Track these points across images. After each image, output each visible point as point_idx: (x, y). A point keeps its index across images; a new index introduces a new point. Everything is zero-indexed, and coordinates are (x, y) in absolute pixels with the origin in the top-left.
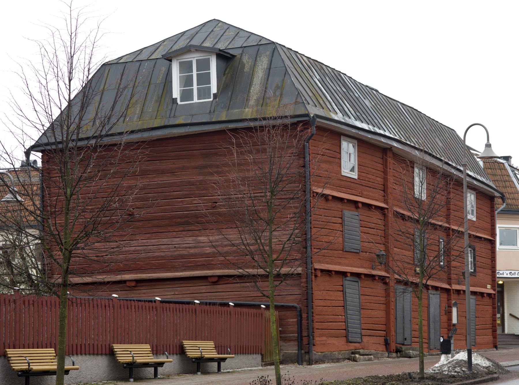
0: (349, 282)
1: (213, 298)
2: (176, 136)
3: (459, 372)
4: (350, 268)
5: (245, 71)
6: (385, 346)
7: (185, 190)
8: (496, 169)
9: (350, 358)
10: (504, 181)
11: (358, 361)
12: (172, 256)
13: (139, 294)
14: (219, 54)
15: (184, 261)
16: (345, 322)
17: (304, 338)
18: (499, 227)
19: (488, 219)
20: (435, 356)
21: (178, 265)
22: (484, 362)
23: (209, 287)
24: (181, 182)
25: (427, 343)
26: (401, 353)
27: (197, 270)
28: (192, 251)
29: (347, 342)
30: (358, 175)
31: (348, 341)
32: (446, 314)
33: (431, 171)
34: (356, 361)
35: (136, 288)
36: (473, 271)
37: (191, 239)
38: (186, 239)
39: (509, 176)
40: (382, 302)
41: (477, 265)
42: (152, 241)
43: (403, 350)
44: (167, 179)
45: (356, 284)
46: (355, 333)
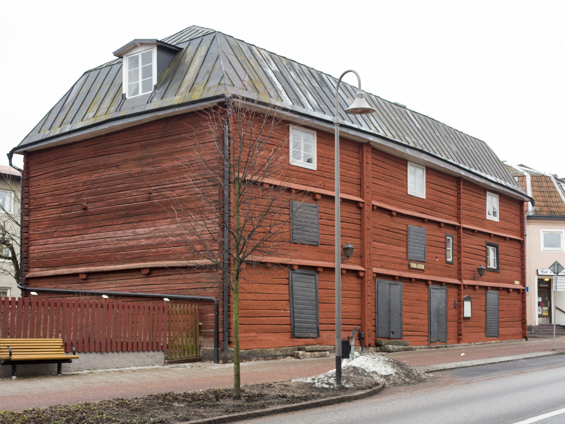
0: (299, 275)
1: (146, 290)
2: (120, 129)
3: (332, 384)
4: (302, 261)
5: (186, 61)
6: (358, 341)
7: (127, 182)
8: (542, 182)
9: (294, 355)
10: (550, 192)
11: (301, 358)
12: (114, 249)
13: (89, 286)
14: (160, 45)
15: (124, 254)
16: (289, 317)
17: (220, 334)
18: (543, 231)
19: (517, 221)
20: (433, 349)
21: (120, 257)
22: (384, 369)
23: (143, 279)
24: (123, 174)
25: (427, 336)
26: (381, 347)
27: (134, 262)
28: (131, 243)
29: (292, 338)
30: (318, 166)
31: (293, 336)
32: (455, 308)
33: (430, 170)
34: (299, 358)
35: (88, 281)
36: (496, 268)
37: (130, 231)
38: (127, 231)
39: (554, 187)
40: (357, 296)
41: (500, 262)
42: (101, 234)
43: (383, 344)
44: (112, 173)
45: (313, 277)
46: (307, 328)
